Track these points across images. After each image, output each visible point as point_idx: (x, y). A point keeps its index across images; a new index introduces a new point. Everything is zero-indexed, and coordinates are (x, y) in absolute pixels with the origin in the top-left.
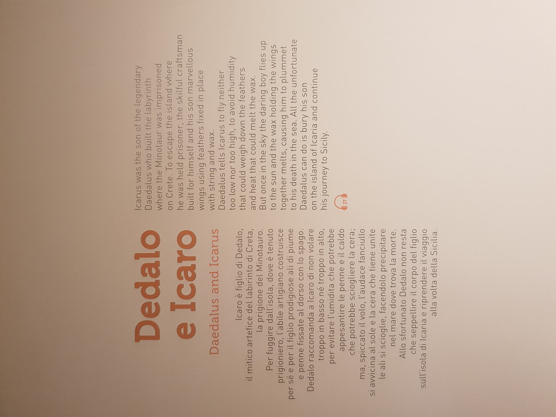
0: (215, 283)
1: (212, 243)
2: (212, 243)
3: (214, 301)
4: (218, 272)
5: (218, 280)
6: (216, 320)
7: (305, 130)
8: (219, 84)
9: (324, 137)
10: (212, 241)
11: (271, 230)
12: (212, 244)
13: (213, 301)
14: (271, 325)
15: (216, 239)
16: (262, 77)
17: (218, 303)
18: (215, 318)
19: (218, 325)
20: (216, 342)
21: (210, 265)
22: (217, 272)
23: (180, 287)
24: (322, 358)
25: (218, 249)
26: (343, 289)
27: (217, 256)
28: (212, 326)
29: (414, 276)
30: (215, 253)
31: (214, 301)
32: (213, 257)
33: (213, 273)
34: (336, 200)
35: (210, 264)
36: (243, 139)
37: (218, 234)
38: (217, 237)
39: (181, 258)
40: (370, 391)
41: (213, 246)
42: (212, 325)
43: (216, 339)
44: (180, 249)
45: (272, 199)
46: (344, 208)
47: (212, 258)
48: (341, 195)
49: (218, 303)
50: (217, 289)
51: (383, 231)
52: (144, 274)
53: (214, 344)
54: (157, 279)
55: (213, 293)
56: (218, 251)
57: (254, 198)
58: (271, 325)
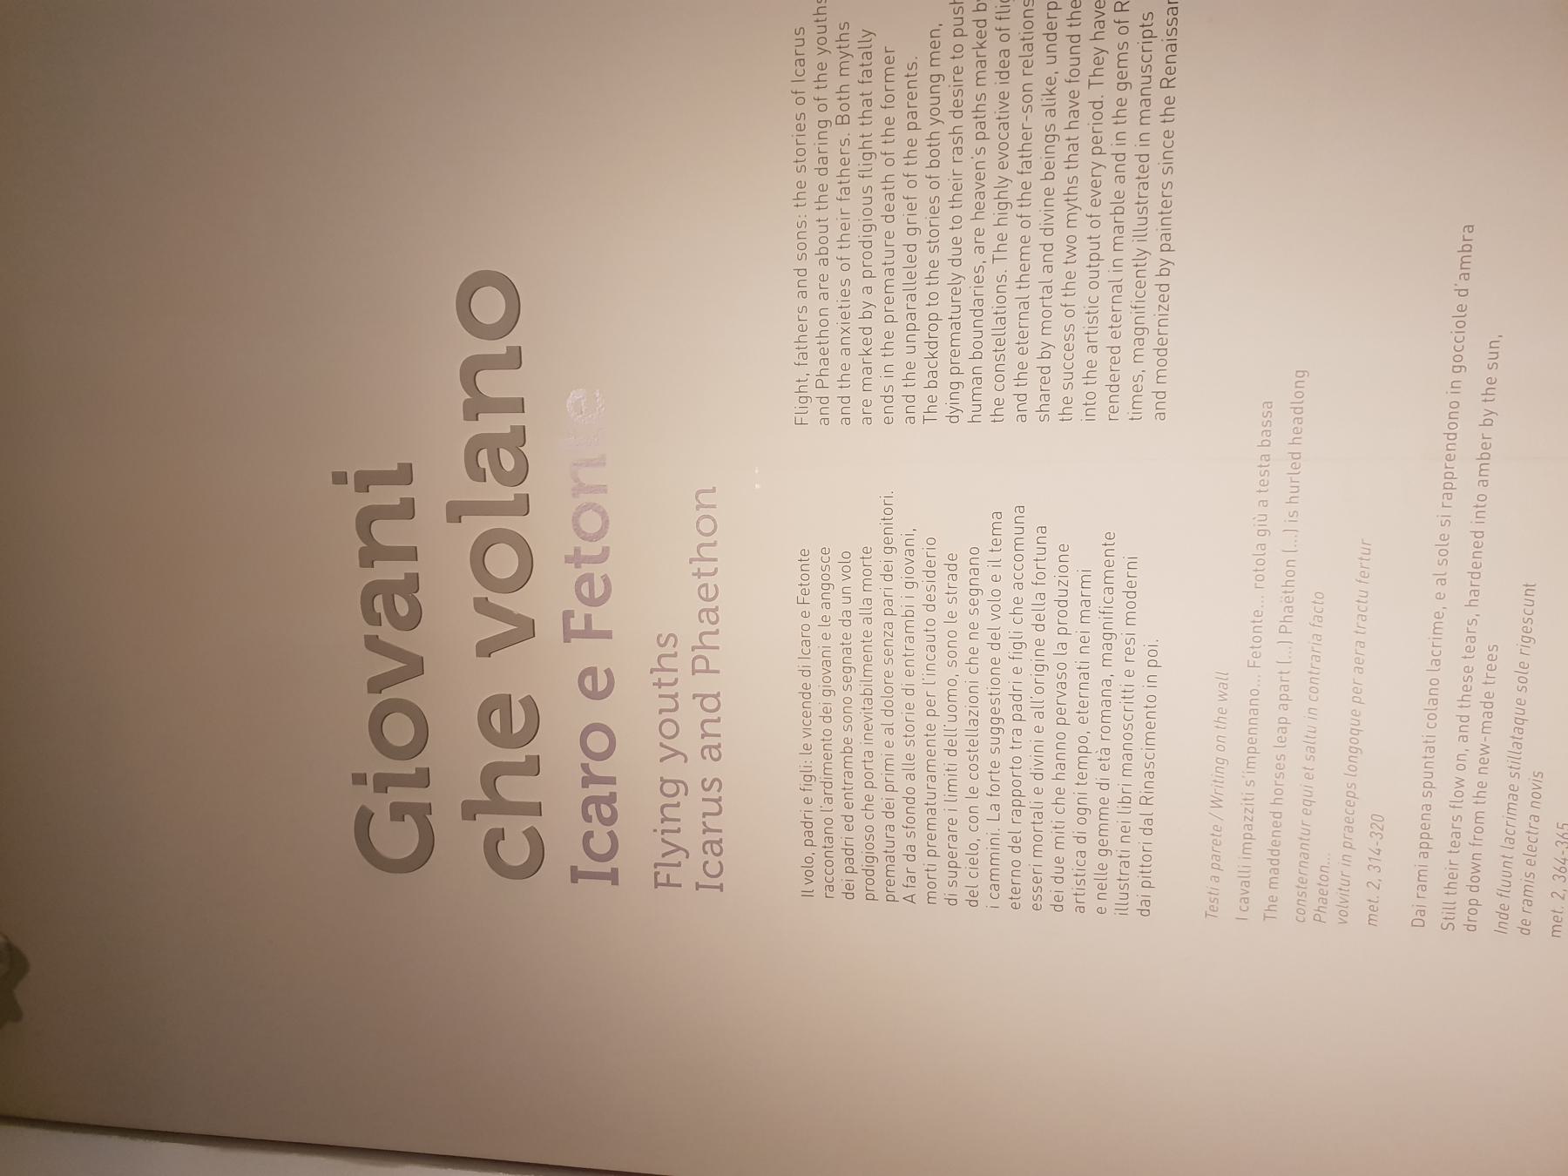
0: (709, 728)
1: (704, 820)
3: (707, 785)
5: (718, 720)
6: (714, 848)
7: (978, 355)
8: (975, 114)
9: (1001, 185)
10: (701, 813)
12: (704, 823)
13: (705, 783)
14: (824, 180)
15: (714, 808)
16: (865, 310)
17: (719, 791)
19: (704, 832)
20: (710, 613)
21: (698, 886)
22: (716, 696)
23: (588, 836)
25: (719, 746)
26: (1064, 631)
27: (720, 862)
28: (700, 698)
30: (712, 851)
31: (707, 785)
32: (707, 862)
33: (705, 697)
35: (697, 883)
36: (1039, 628)
37: (720, 794)
38: (718, 801)
39: (589, 779)
40: (1120, 822)
41: (674, 697)
43: (711, 605)
44: (587, 760)
45: (994, 421)
47: (704, 866)
49: (719, 791)
50: (718, 747)
52: (477, 474)
54: (521, 490)
55: (704, 758)
56: (721, 803)
57: (1145, 884)
58: (824, 180)
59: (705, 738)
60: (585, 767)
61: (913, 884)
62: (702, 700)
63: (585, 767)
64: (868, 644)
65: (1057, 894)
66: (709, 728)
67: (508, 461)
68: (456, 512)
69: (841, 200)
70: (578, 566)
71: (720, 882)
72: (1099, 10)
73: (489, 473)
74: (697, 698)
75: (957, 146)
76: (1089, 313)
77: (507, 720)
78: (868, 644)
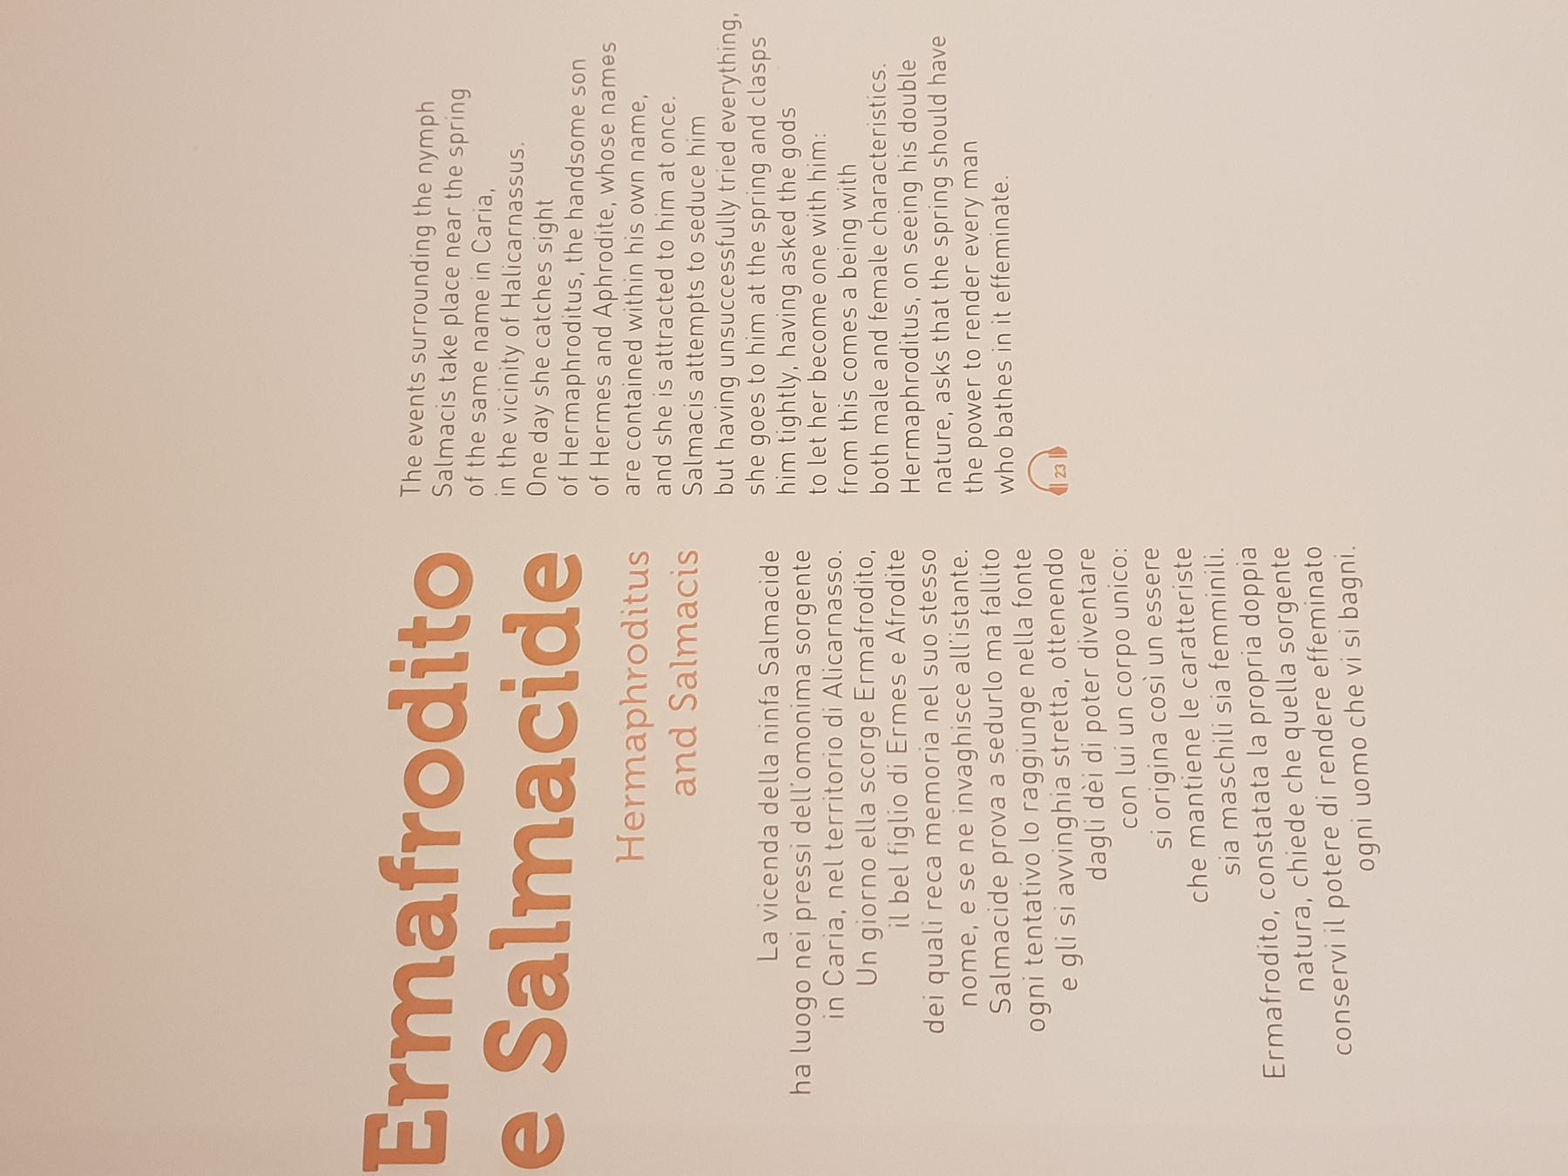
0: (684, 762)
2: (627, 792)
4: (695, 729)
5: (693, 754)
8: (842, 178)
11: (992, 554)
12: (627, 797)
18: (686, 676)
24: (730, 185)
28: (676, 733)
29: (1123, 660)
30: (686, 791)
31: (634, 559)
33: (681, 731)
34: (1033, 463)
42: (627, 623)
43: (691, 600)
46: (1059, 490)
48: (1049, 452)
50: (692, 782)
51: (1087, 555)
53: (683, 684)
54: (566, 814)
59: (680, 773)
60: (411, 820)
61: (996, 609)
62: (678, 736)
63: (411, 820)
64: (546, 207)
65: (1093, 779)
66: (684, 762)
67: (556, 789)
68: (499, 939)
69: (987, 613)
70: (630, 603)
71: (645, 682)
72: (973, 402)
73: (538, 801)
74: (673, 733)
75: (758, 74)
76: (873, 105)
77: (531, 1138)
78: (546, 207)
